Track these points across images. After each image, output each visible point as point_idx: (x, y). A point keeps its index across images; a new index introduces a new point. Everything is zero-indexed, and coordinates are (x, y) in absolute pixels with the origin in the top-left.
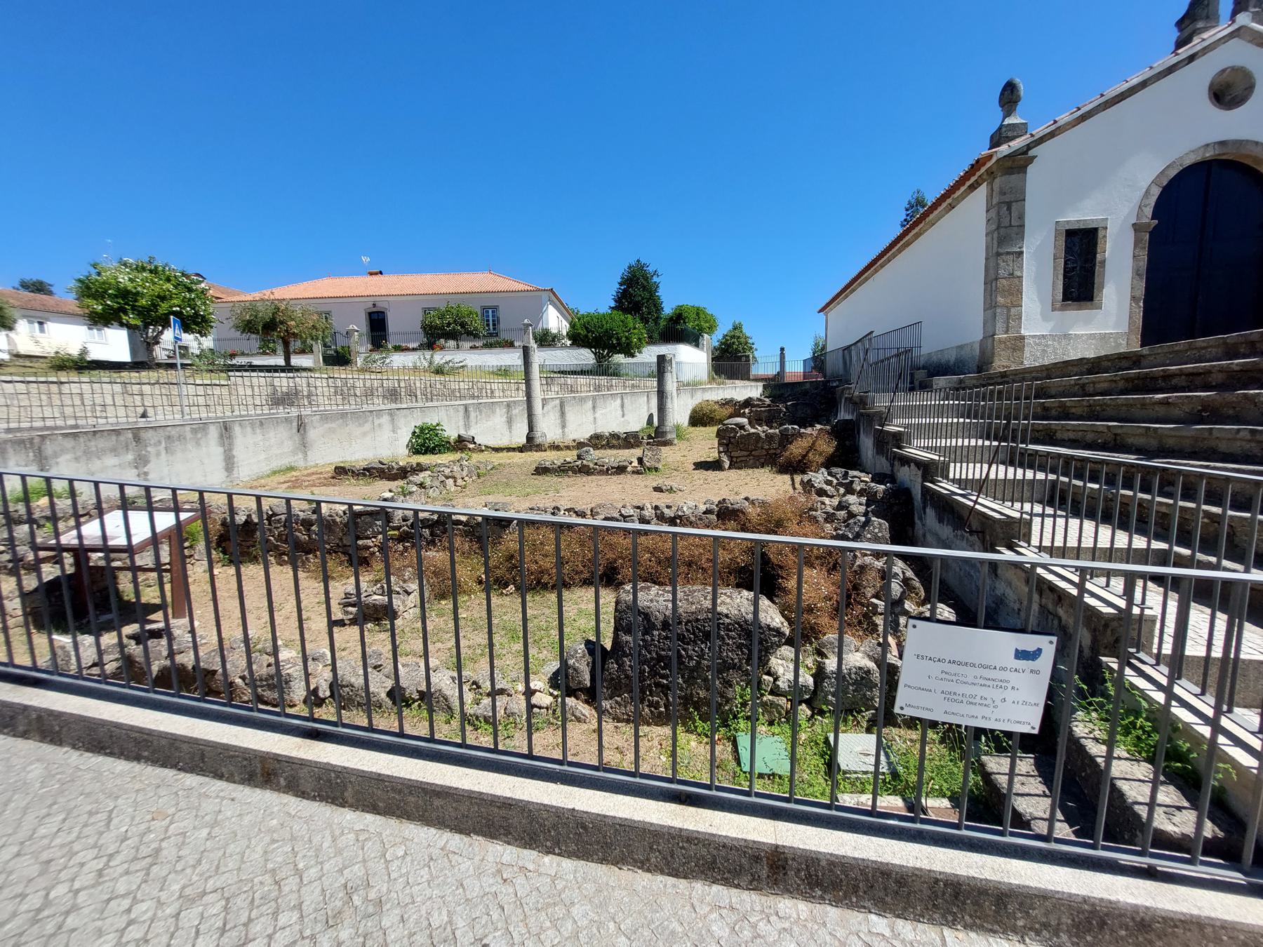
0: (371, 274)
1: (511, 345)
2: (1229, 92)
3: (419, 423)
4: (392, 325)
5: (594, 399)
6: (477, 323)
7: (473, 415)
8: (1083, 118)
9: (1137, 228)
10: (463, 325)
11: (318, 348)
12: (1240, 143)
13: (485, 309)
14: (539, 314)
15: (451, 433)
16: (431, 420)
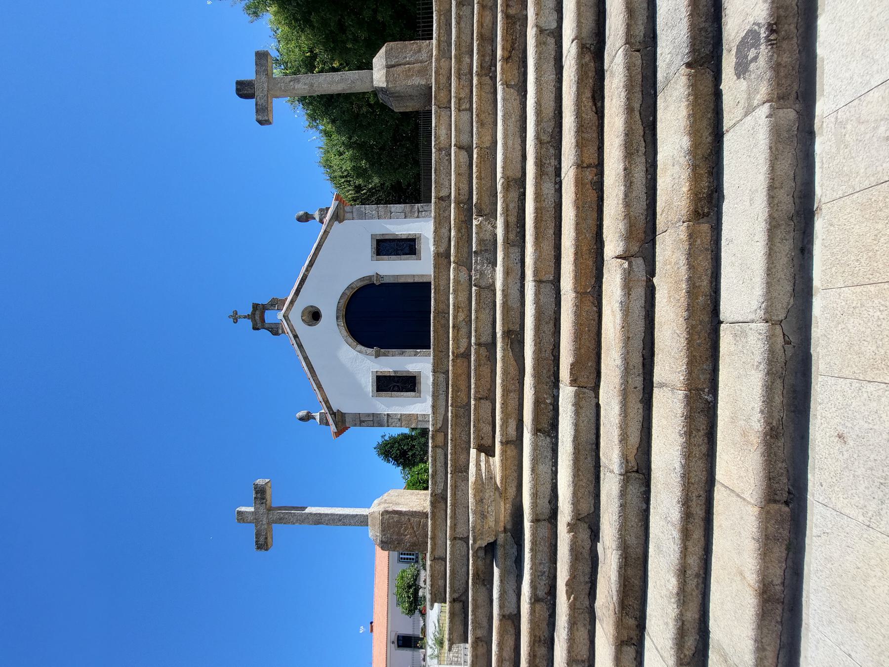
0: (372, 630)
2: (314, 316)
9: (377, 355)
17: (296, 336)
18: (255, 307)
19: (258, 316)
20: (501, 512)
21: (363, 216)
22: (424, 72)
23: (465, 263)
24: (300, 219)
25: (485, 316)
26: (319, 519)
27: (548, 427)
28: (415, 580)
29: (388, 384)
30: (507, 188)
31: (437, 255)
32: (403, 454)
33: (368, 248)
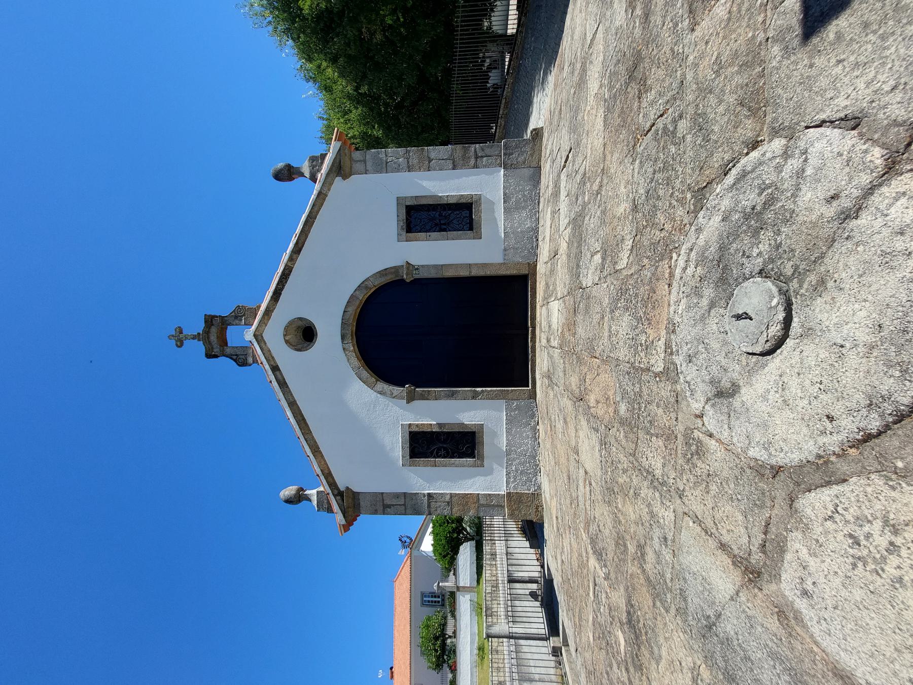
0: (392, 677)
2: (305, 334)
13: (423, 603)
17: (275, 369)
18: (210, 320)
19: (215, 336)
21: (383, 167)
29: (425, 445)
33: (391, 220)
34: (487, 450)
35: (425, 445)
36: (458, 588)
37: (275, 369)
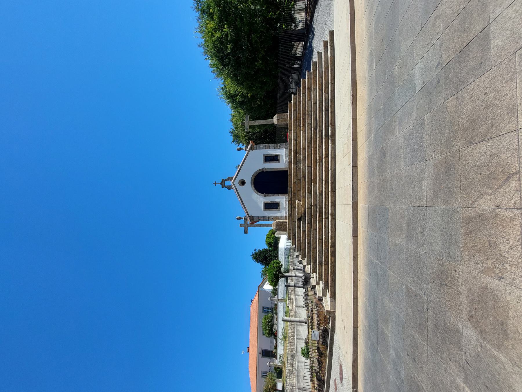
0: (248, 351)
1: (276, 305)
2: (243, 183)
3: (301, 354)
4: (267, 348)
5: (296, 295)
6: (269, 316)
7: (299, 337)
8: (245, 207)
10: (269, 322)
11: (277, 380)
12: (251, 180)
13: (264, 312)
14: (266, 292)
15: (304, 345)
16: (300, 350)
17: (237, 190)
18: (223, 180)
19: (223, 183)
20: (303, 210)
21: (260, 148)
22: (286, 120)
23: (295, 164)
24: (238, 150)
25: (299, 174)
26: (260, 226)
27: (310, 192)
28: (272, 319)
29: (268, 206)
30: (303, 150)
31: (289, 162)
32: (266, 258)
33: (262, 159)
34: (281, 207)
35: (268, 206)
36: (278, 300)
37: (237, 190)
